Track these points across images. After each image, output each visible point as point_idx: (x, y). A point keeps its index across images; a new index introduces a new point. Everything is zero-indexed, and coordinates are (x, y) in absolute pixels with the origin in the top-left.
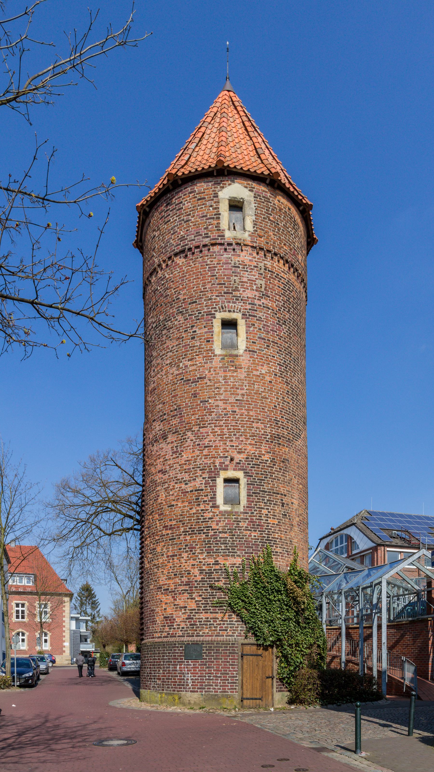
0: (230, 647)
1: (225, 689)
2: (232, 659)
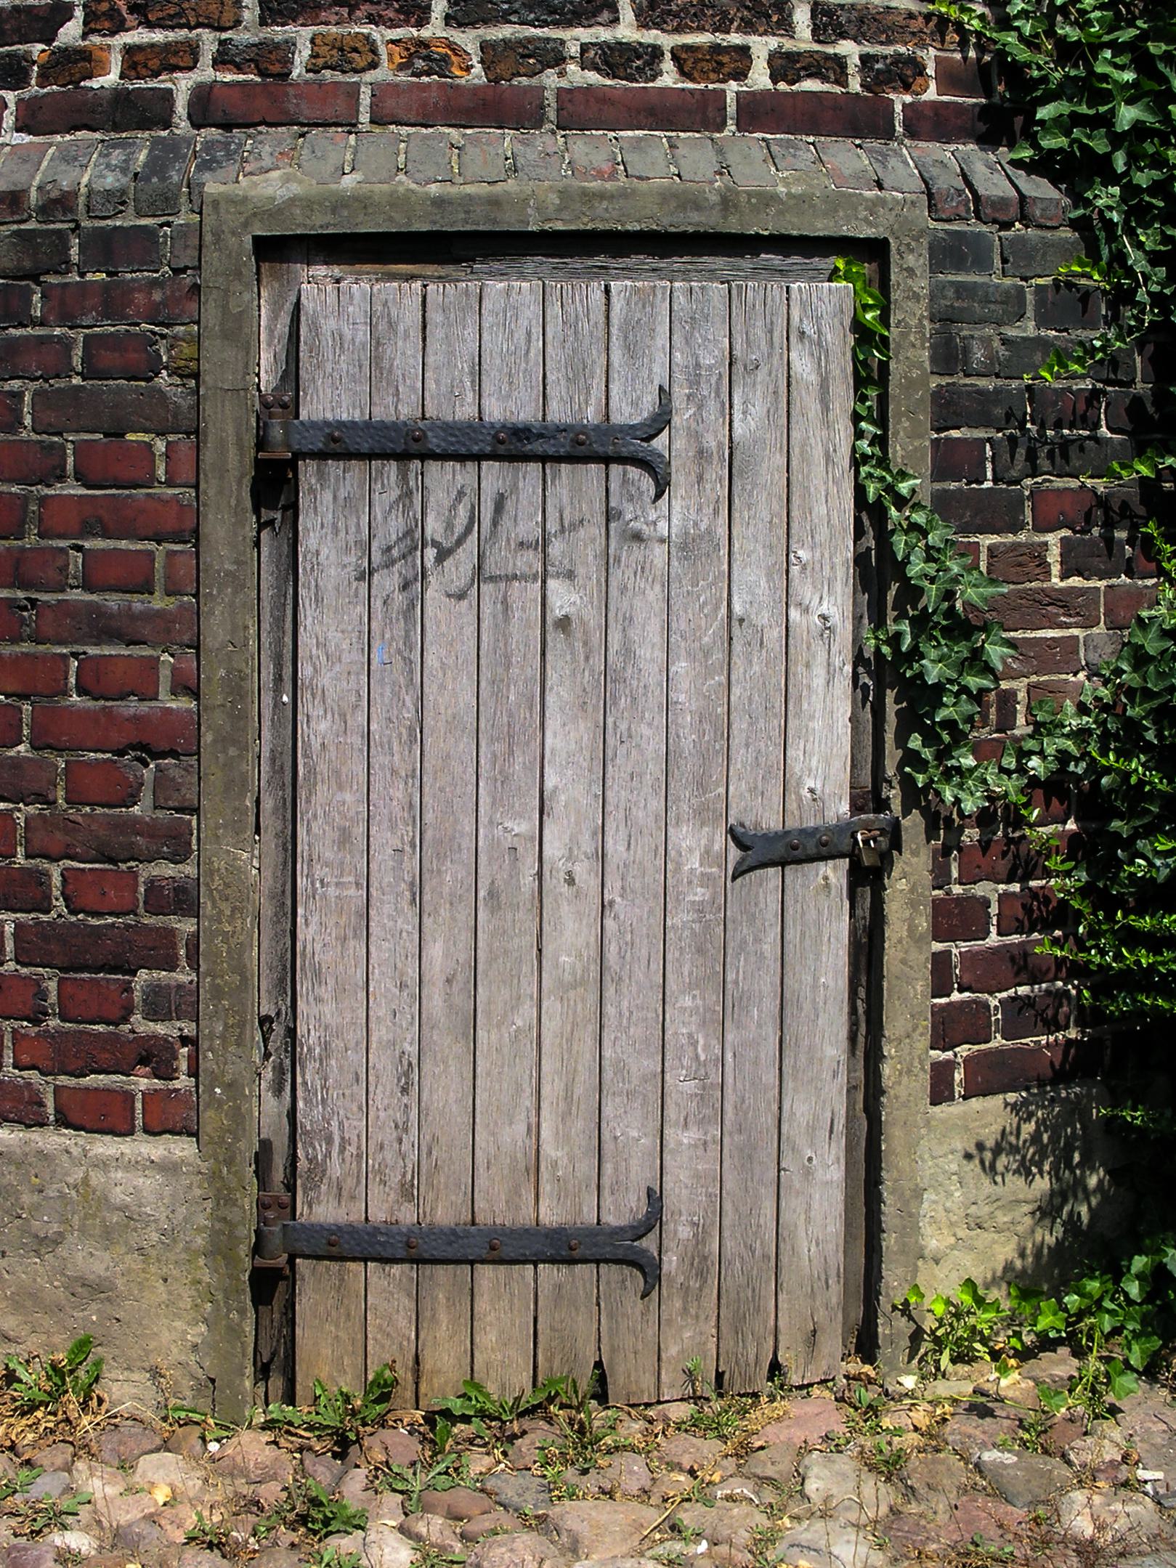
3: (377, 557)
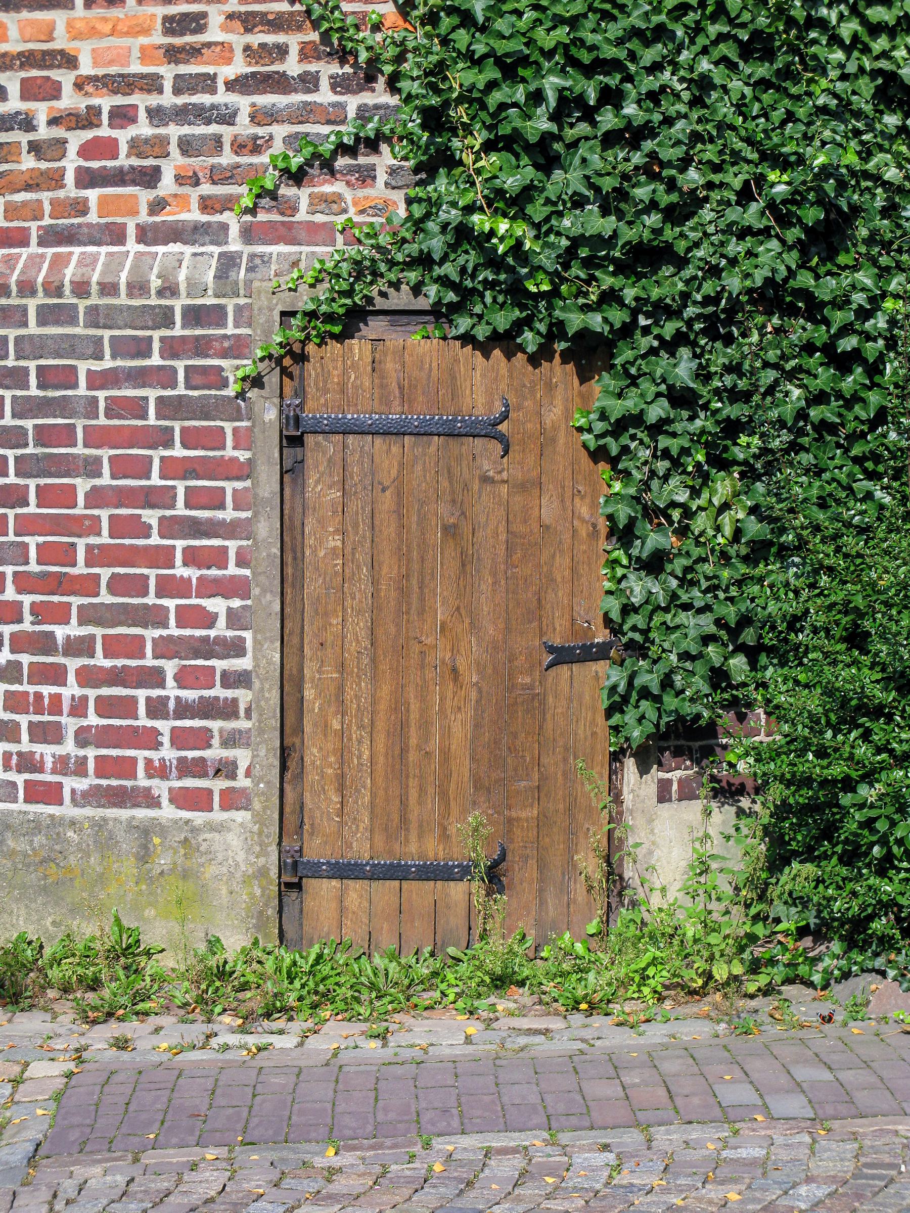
0: (172, 348)
1: (127, 768)
2: (186, 469)
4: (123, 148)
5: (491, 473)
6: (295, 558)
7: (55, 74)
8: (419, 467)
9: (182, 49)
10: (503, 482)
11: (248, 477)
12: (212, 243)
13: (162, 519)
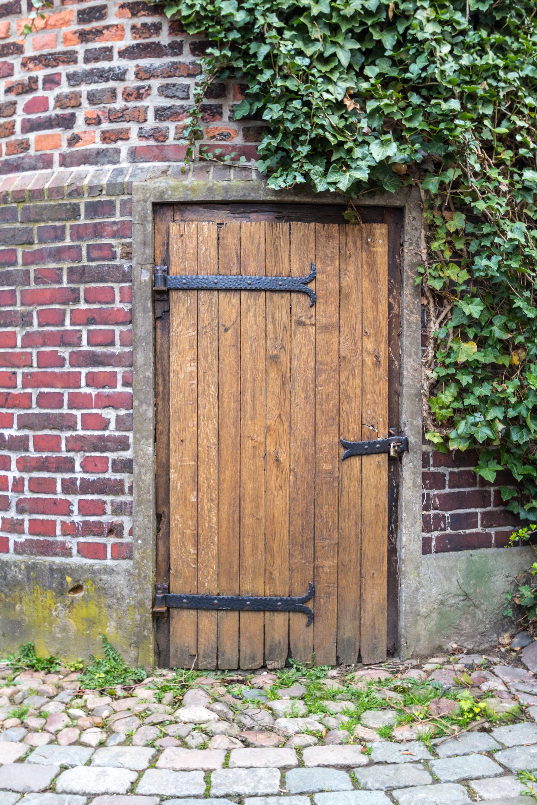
0: (79, 233)
3: (305, 99)
4: (52, 103)
5: (303, 319)
6: (164, 380)
7: (9, 59)
8: (251, 314)
9: (90, 32)
10: (312, 325)
11: (131, 322)
12: (109, 162)
13: (72, 354)
